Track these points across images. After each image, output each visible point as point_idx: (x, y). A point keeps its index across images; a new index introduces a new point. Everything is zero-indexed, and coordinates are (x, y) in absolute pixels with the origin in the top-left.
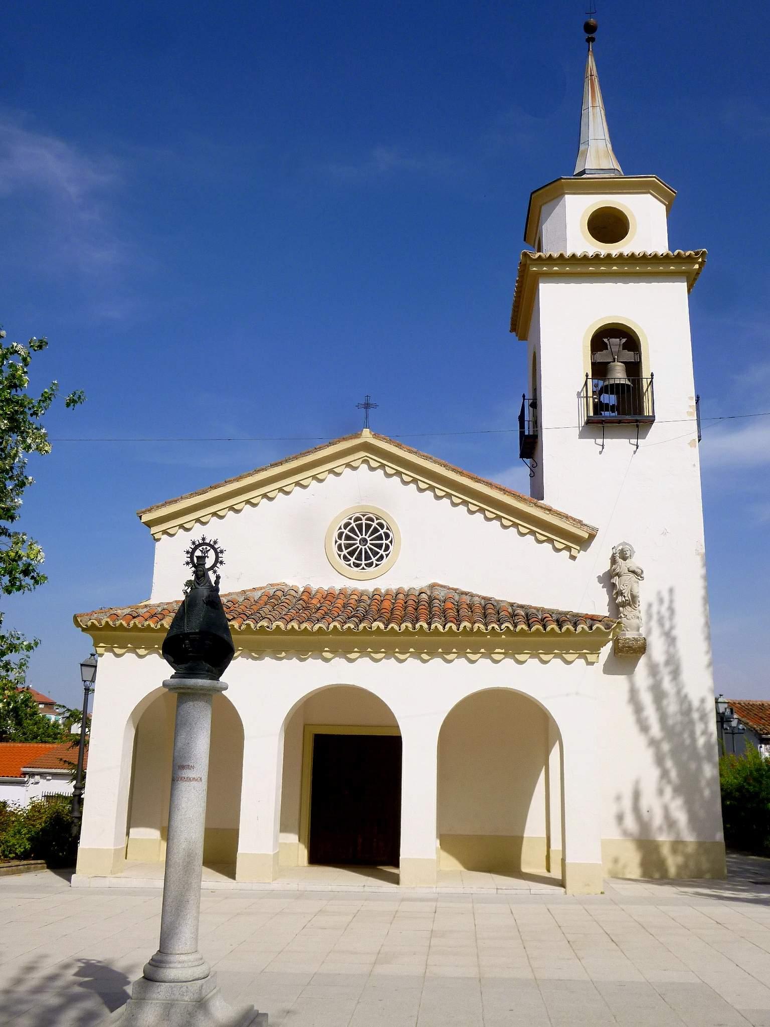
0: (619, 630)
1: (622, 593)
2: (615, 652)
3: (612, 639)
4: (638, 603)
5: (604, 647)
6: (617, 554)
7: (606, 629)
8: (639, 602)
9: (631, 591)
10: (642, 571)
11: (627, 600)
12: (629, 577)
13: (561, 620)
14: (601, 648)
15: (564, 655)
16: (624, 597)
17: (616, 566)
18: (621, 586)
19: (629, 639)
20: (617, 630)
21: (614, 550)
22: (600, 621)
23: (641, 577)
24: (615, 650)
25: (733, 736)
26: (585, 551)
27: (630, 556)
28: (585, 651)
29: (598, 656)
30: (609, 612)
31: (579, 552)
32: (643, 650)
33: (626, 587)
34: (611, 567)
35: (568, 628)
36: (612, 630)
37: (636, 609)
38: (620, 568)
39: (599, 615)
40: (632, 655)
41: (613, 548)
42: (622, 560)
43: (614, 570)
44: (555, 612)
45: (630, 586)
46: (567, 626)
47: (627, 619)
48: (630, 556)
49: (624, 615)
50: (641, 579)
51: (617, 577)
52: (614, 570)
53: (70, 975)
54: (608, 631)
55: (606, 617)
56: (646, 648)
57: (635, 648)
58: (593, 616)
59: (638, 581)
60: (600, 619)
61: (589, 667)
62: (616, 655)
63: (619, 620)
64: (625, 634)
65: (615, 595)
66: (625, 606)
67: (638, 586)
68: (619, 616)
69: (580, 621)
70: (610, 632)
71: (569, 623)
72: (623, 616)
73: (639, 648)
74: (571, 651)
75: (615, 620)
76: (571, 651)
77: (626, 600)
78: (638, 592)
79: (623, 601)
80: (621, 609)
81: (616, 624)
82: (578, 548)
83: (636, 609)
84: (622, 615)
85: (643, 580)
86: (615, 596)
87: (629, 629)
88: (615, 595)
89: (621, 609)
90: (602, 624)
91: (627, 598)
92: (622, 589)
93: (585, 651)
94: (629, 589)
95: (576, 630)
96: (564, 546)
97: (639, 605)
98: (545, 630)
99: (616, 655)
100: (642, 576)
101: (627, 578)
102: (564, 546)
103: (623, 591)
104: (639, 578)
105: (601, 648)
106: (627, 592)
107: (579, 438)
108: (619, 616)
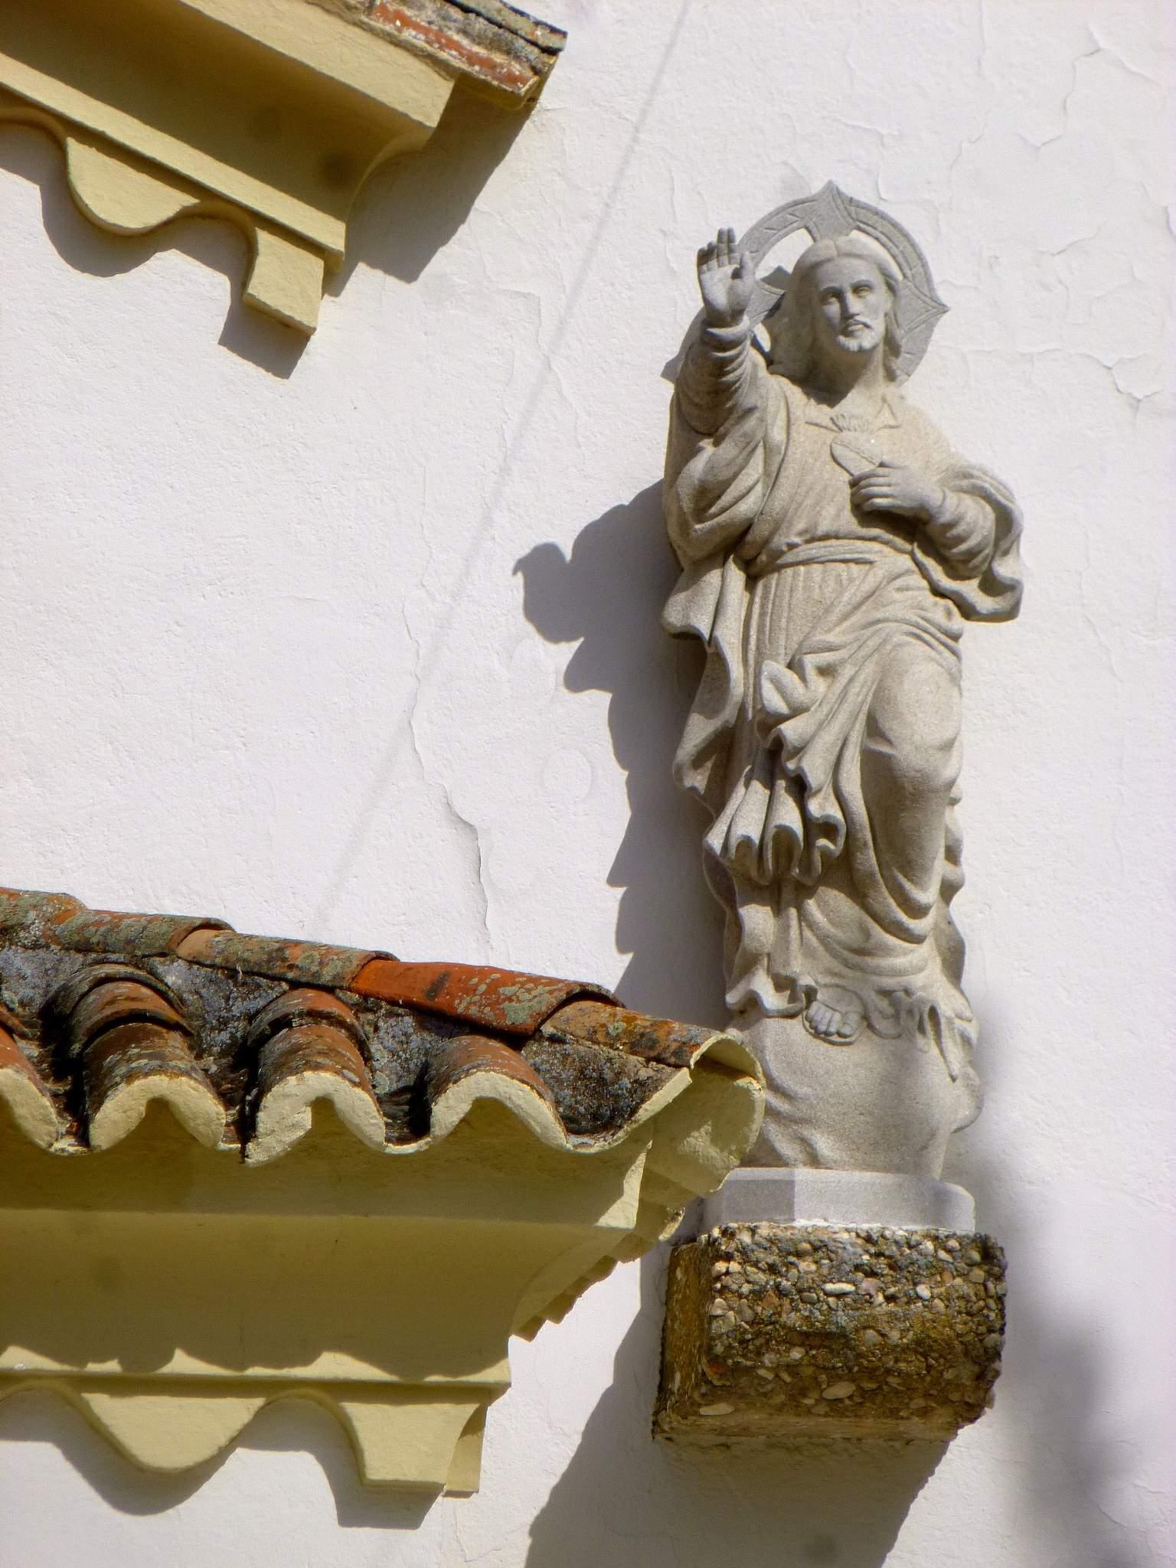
0: (716, 1139)
1: (779, 744)
2: (662, 1388)
3: (631, 1245)
4: (940, 868)
5: (548, 1325)
6: (753, 327)
7: (572, 1124)
8: (953, 855)
9: (874, 728)
10: (1006, 523)
11: (828, 829)
12: (862, 581)
13: (93, 1010)
14: (515, 1342)
15: (102, 1404)
16: (800, 789)
17: (729, 449)
18: (775, 667)
19: (820, 1248)
20: (699, 1141)
21: (720, 274)
22: (516, 1039)
23: (992, 585)
24: (665, 1372)
25: (852, 475)
26: (406, 266)
27: (891, 345)
28: (333, 1365)
29: (475, 1425)
30: (622, 948)
31: (334, 278)
32: (965, 1372)
33: (819, 685)
34: (681, 452)
35: (159, 1107)
36: (636, 1140)
37: (916, 925)
38: (772, 478)
39: (509, 977)
40: (837, 1428)
41: (705, 257)
42: (796, 393)
43: (708, 494)
44: (36, 930)
45: (869, 670)
46: (159, 1084)
47: (819, 1034)
48: (891, 345)
49: (783, 983)
50: (984, 603)
51: (736, 576)
52: (708, 494)
53: (714, 1369)
54: (596, 1145)
55: (586, 994)
56: (995, 1354)
57: (887, 1348)
58: (444, 976)
59: (958, 622)
60: (518, 1015)
61: (368, 1538)
62: (670, 1419)
63: (732, 1034)
64: (782, 1198)
65: (697, 762)
66: (804, 890)
67: (955, 678)
68: (732, 998)
69: (298, 1036)
70: (613, 1167)
71: (175, 1043)
72: (771, 999)
73: (922, 1347)
74: (182, 1363)
75: (679, 1030)
76: (182, 1363)
77: (816, 827)
78: (947, 746)
79: (784, 833)
80: (757, 918)
81: (682, 1079)
82: (331, 232)
83: (916, 925)
84: (762, 985)
85: (1010, 614)
86: (698, 780)
87: (824, 1144)
88: (697, 762)
89: (757, 918)
90: (541, 1079)
91: (822, 806)
92: (774, 701)
93: (333, 1365)
94: (859, 696)
95: (245, 1128)
96: (177, 201)
97: (949, 890)
98: (82, 1135)
99: (670, 1419)
100: (1004, 569)
101: (841, 587)
102: (177, 201)
103: (791, 730)
104: (970, 589)
105: (515, 1342)
106: (828, 740)
107: (830, 182)
108: (732, 998)
